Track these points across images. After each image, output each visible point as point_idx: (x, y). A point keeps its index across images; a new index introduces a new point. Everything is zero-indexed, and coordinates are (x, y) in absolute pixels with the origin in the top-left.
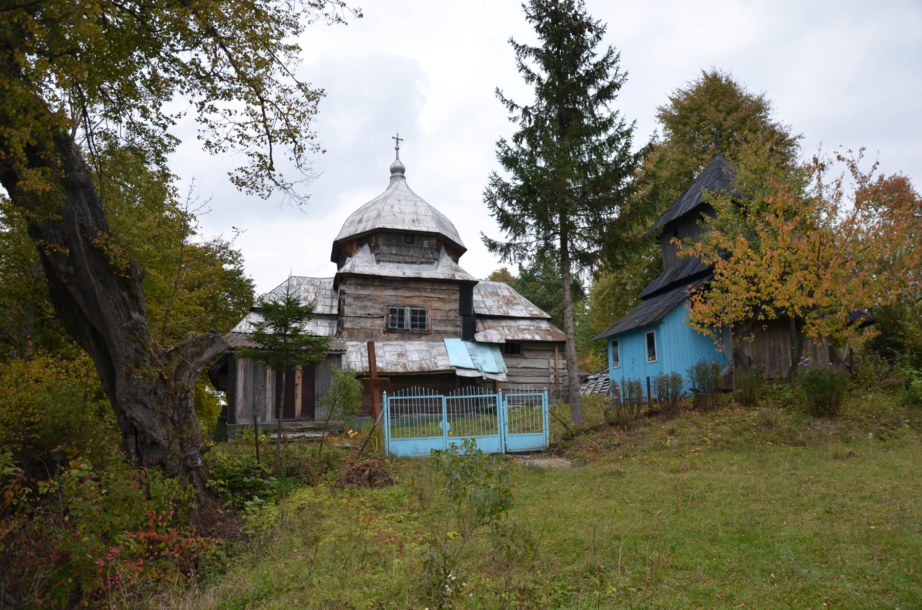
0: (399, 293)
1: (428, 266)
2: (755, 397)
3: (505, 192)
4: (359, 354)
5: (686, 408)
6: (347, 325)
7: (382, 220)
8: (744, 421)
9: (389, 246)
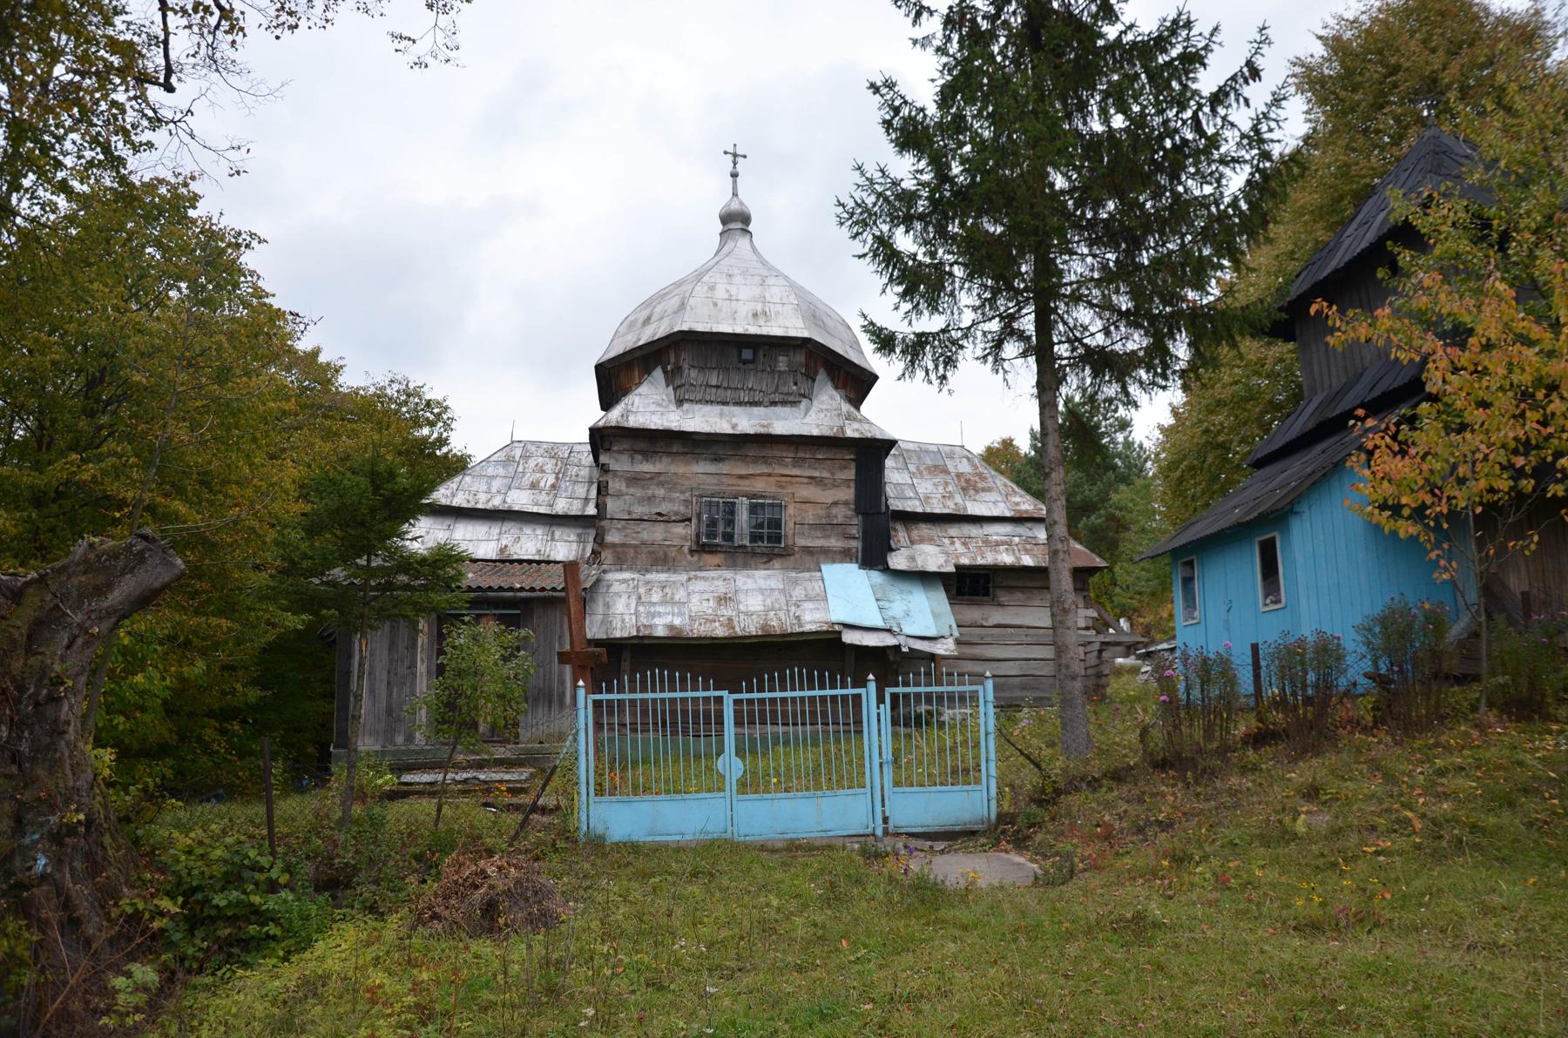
0: (725, 468)
1: (787, 410)
2: (1544, 696)
3: (900, 206)
4: (634, 597)
5: (1355, 724)
6: (613, 537)
7: (687, 315)
8: (1520, 764)
9: (702, 369)
